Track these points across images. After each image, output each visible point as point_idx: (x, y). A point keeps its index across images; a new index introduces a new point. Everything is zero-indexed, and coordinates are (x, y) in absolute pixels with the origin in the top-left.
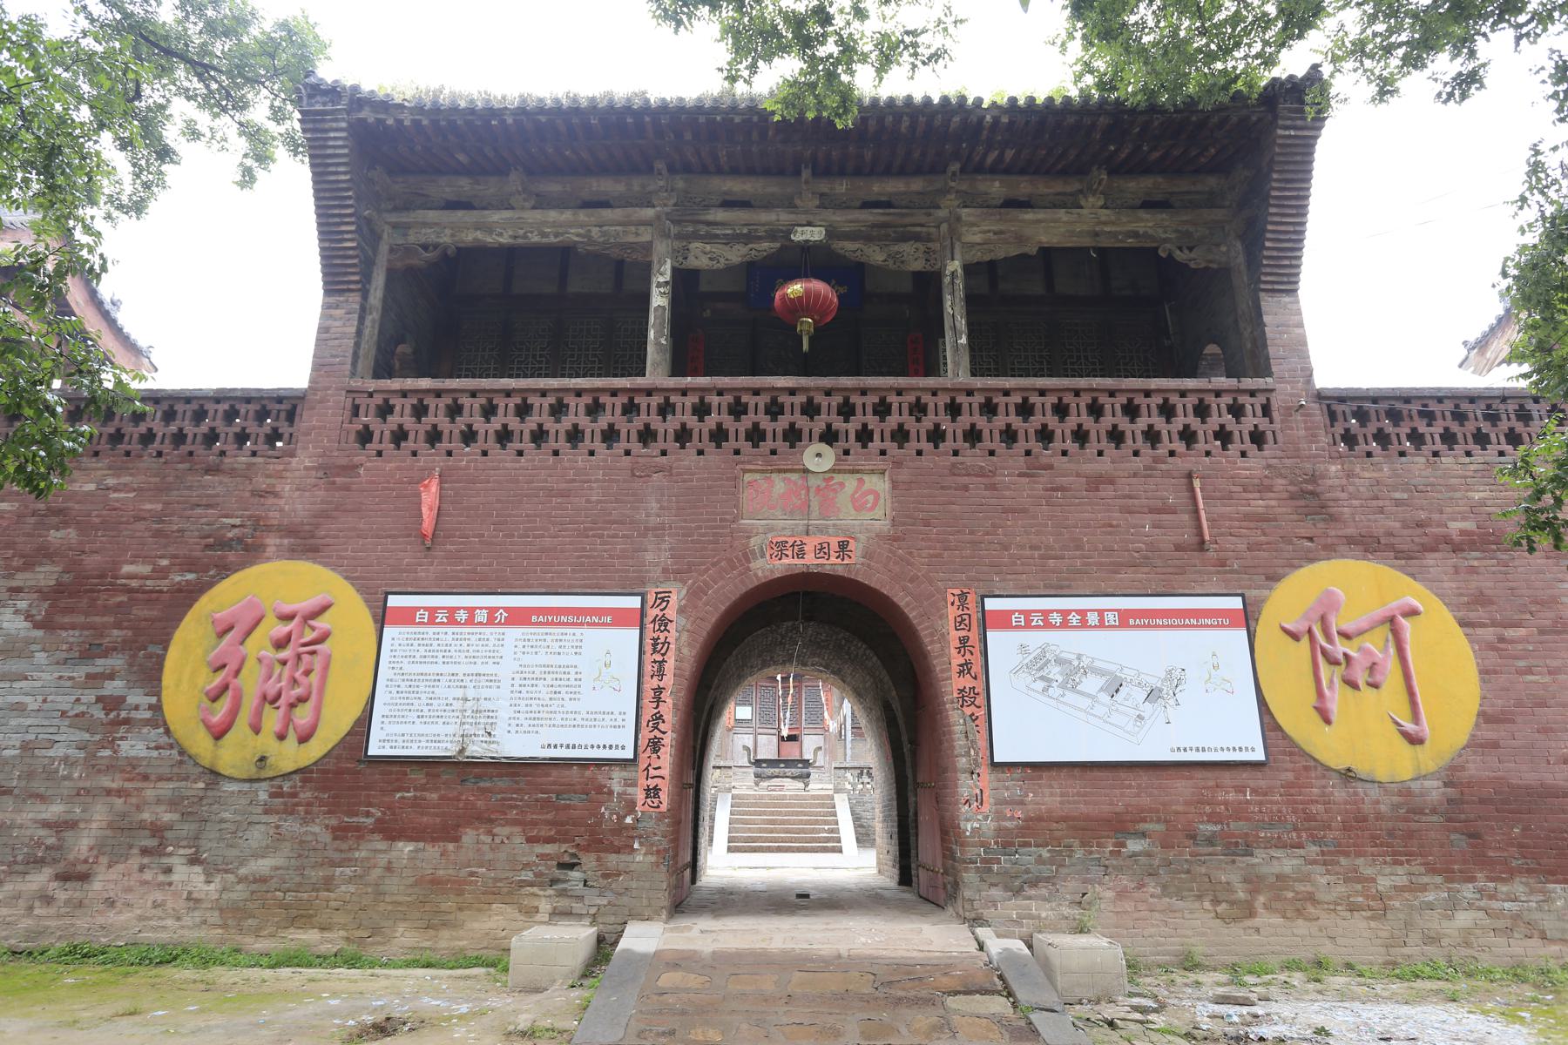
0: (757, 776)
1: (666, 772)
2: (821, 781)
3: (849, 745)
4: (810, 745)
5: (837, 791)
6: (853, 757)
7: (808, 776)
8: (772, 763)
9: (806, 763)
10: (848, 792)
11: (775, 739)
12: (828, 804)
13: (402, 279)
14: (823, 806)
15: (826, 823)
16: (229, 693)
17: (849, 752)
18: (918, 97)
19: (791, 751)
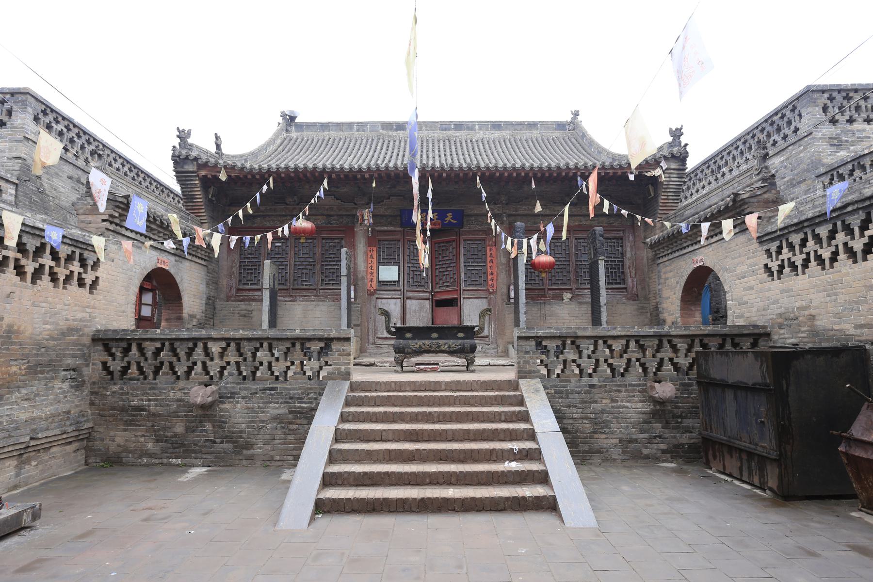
0: (397, 350)
1: (714, 434)
2: (485, 355)
3: (522, 309)
4: (471, 311)
5: (523, 374)
6: (529, 326)
7: (473, 349)
8: (420, 332)
9: (470, 332)
10: (541, 377)
11: (427, 304)
12: (510, 396)
13: (457, 305)
14: (502, 401)
15: (512, 436)
16: (357, 361)
17: (523, 317)
18: (518, 165)
19: (447, 317)
